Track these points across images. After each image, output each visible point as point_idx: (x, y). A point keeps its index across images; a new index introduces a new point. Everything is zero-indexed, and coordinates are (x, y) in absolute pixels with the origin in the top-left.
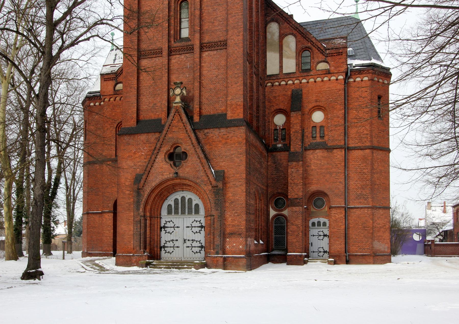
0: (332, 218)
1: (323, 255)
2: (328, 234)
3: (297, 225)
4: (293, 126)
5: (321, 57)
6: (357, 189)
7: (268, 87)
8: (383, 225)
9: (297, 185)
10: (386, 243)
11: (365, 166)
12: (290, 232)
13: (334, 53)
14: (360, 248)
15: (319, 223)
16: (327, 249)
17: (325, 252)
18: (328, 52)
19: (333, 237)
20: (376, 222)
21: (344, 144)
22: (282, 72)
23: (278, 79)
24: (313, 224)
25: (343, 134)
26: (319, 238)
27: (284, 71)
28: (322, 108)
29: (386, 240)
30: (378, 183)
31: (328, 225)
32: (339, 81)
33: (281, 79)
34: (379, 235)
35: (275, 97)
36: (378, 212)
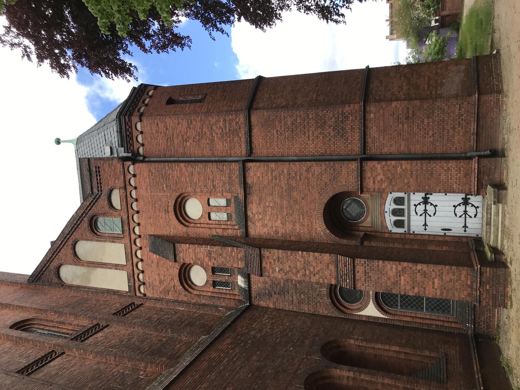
0: (383, 187)
1: (473, 205)
2: (423, 195)
3: (399, 274)
4: (199, 260)
5: (103, 202)
6: (325, 137)
7: (146, 293)
8: (403, 79)
9: (307, 263)
10: (447, 70)
11: (280, 122)
12: (416, 290)
13: (97, 179)
14: (457, 126)
15: (395, 212)
16: (458, 198)
17: (466, 202)
18: (95, 191)
19: (429, 186)
20: (396, 92)
21: (237, 164)
22: (123, 266)
23: (134, 275)
24: (399, 224)
25: (220, 165)
26: (432, 215)
27: (123, 261)
28: (179, 202)
29: (439, 71)
30: (315, 96)
31: (401, 195)
32: (137, 172)
33: (133, 270)
34: (426, 87)
35: (161, 282)
36: (374, 92)
